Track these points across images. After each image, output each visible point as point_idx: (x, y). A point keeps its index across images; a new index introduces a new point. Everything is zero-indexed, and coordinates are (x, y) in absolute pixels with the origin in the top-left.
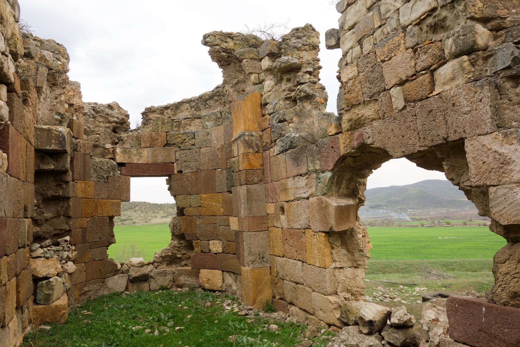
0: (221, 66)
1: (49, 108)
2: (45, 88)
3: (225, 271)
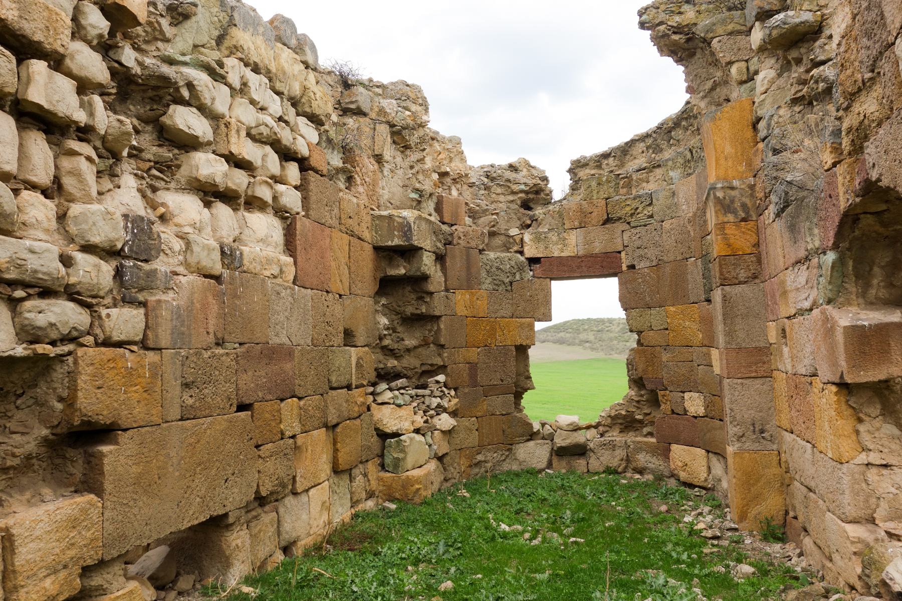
0: (679, 61)
1: (401, 184)
2: (389, 152)
3: (712, 452)
